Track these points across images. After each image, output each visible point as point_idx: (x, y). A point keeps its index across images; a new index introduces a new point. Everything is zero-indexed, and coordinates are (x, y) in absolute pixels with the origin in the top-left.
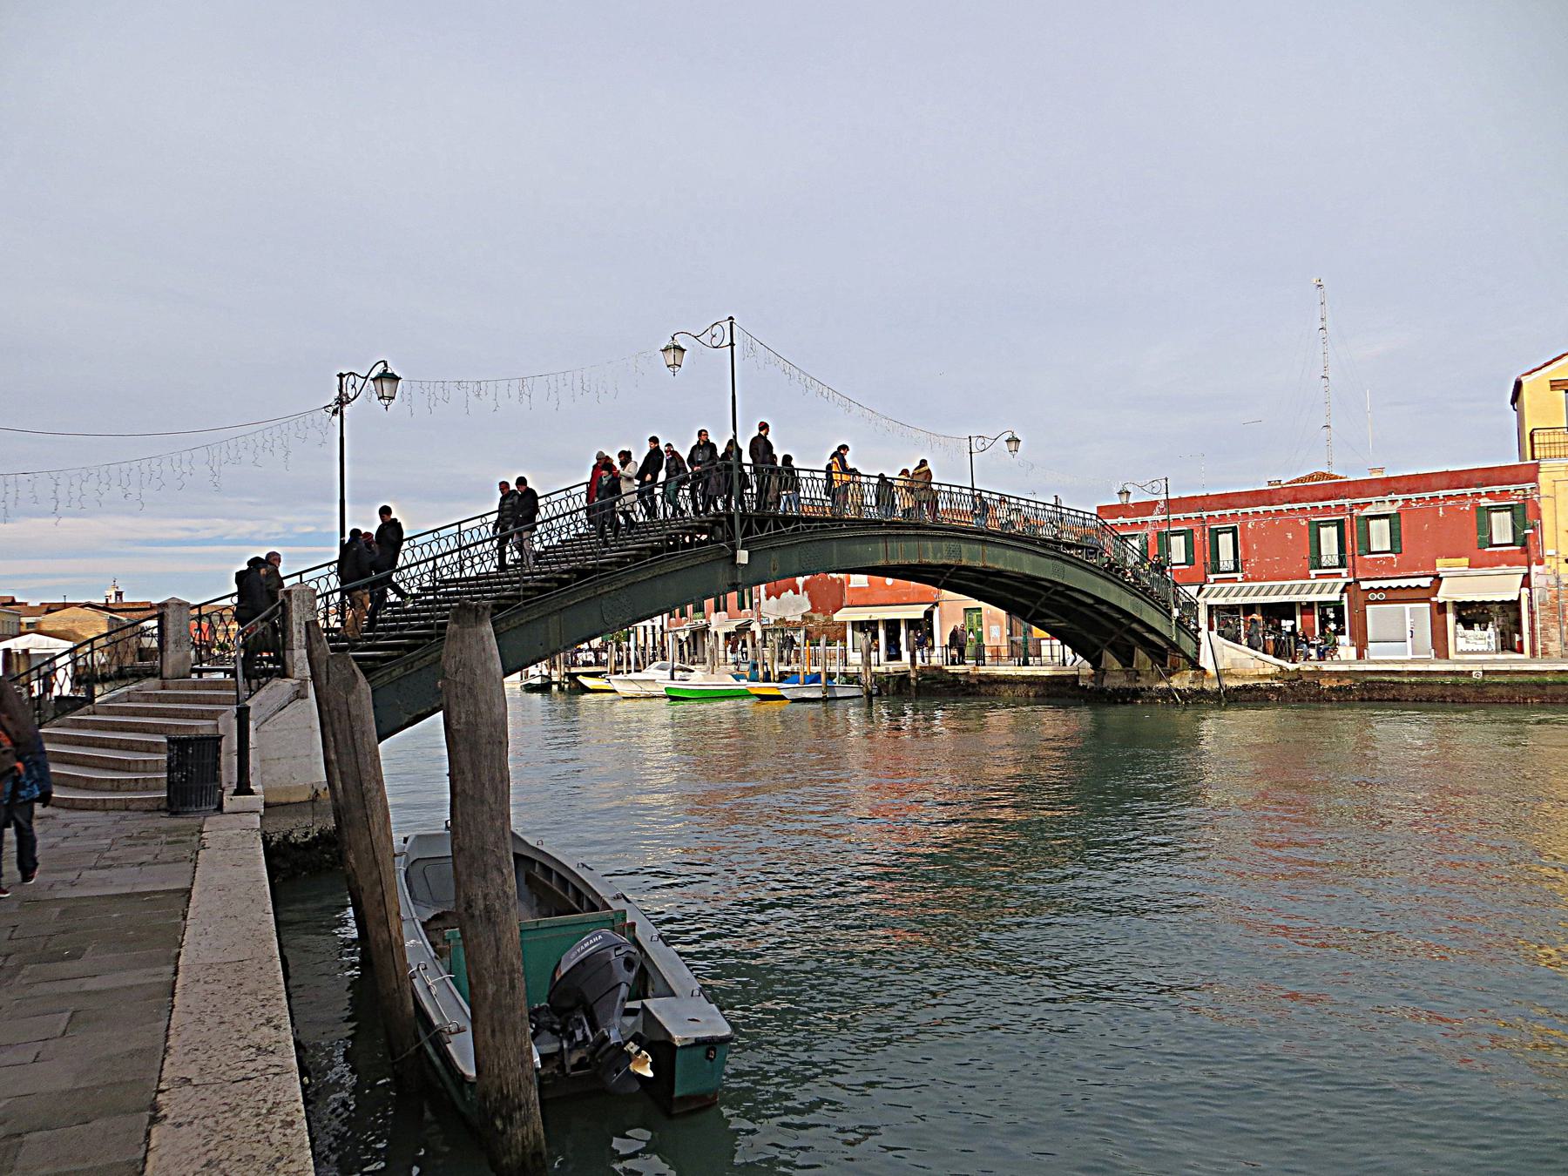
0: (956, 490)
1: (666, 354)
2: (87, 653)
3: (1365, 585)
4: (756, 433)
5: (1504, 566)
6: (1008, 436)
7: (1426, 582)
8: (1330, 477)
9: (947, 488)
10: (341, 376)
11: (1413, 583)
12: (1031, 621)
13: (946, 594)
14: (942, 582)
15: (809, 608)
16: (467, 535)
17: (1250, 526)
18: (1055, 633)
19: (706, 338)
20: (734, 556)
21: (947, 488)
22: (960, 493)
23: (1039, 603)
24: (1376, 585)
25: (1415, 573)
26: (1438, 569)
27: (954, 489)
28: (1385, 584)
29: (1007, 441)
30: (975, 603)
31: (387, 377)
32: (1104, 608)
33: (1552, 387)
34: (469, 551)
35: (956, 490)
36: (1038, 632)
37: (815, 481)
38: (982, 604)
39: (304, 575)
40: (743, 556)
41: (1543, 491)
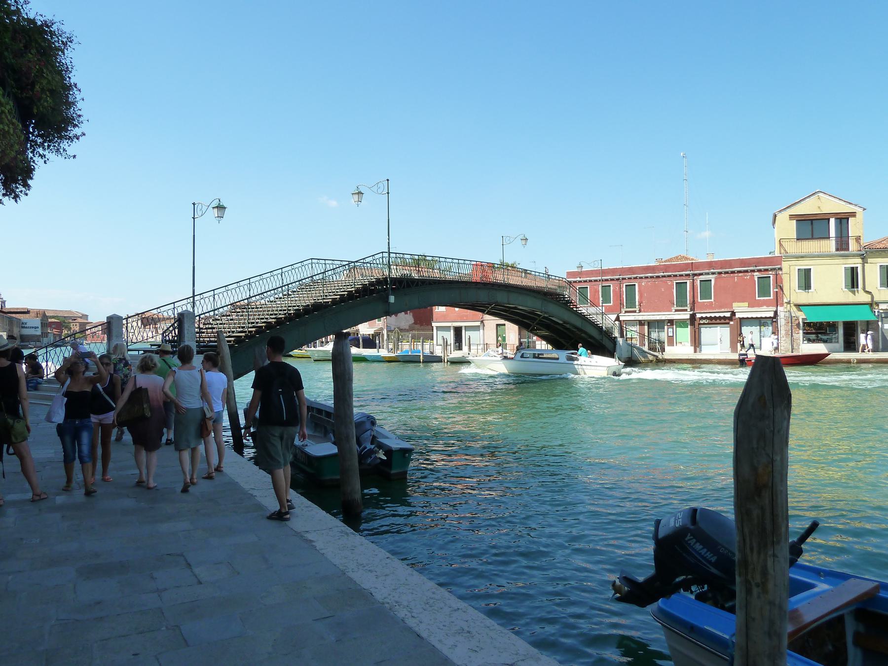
0: (462, 262)
1: (354, 196)
2: (172, 331)
3: (698, 316)
4: (871, 353)
5: (765, 307)
6: (522, 237)
7: (728, 315)
8: (687, 259)
9: (457, 261)
10: (194, 204)
11: (722, 315)
12: (531, 331)
13: (487, 317)
14: (487, 311)
15: (413, 322)
16: (328, 265)
17: (643, 284)
18: (543, 338)
19: (375, 189)
20: (388, 298)
21: (457, 261)
22: (464, 263)
23: (535, 323)
24: (704, 315)
25: (723, 310)
26: (734, 308)
27: (441, 260)
28: (708, 315)
29: (521, 239)
30: (502, 322)
31: (221, 208)
32: (568, 326)
33: (790, 218)
34: (264, 295)
35: (462, 262)
36: (535, 338)
37: (449, 263)
38: (506, 323)
39: (215, 291)
40: (392, 299)
41: (784, 270)
